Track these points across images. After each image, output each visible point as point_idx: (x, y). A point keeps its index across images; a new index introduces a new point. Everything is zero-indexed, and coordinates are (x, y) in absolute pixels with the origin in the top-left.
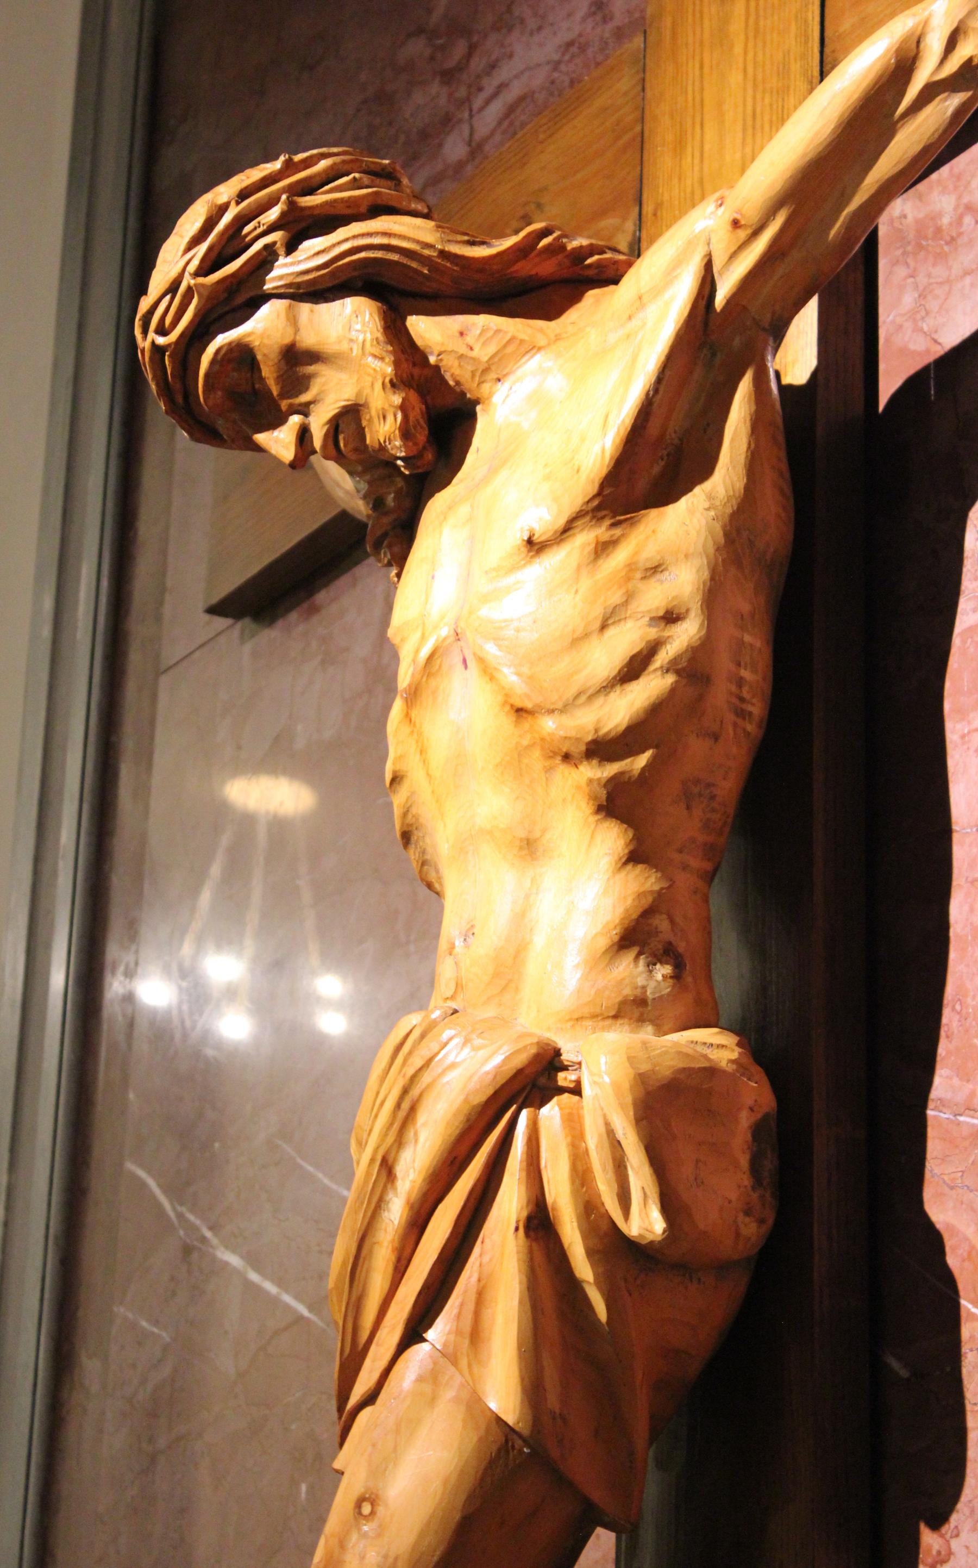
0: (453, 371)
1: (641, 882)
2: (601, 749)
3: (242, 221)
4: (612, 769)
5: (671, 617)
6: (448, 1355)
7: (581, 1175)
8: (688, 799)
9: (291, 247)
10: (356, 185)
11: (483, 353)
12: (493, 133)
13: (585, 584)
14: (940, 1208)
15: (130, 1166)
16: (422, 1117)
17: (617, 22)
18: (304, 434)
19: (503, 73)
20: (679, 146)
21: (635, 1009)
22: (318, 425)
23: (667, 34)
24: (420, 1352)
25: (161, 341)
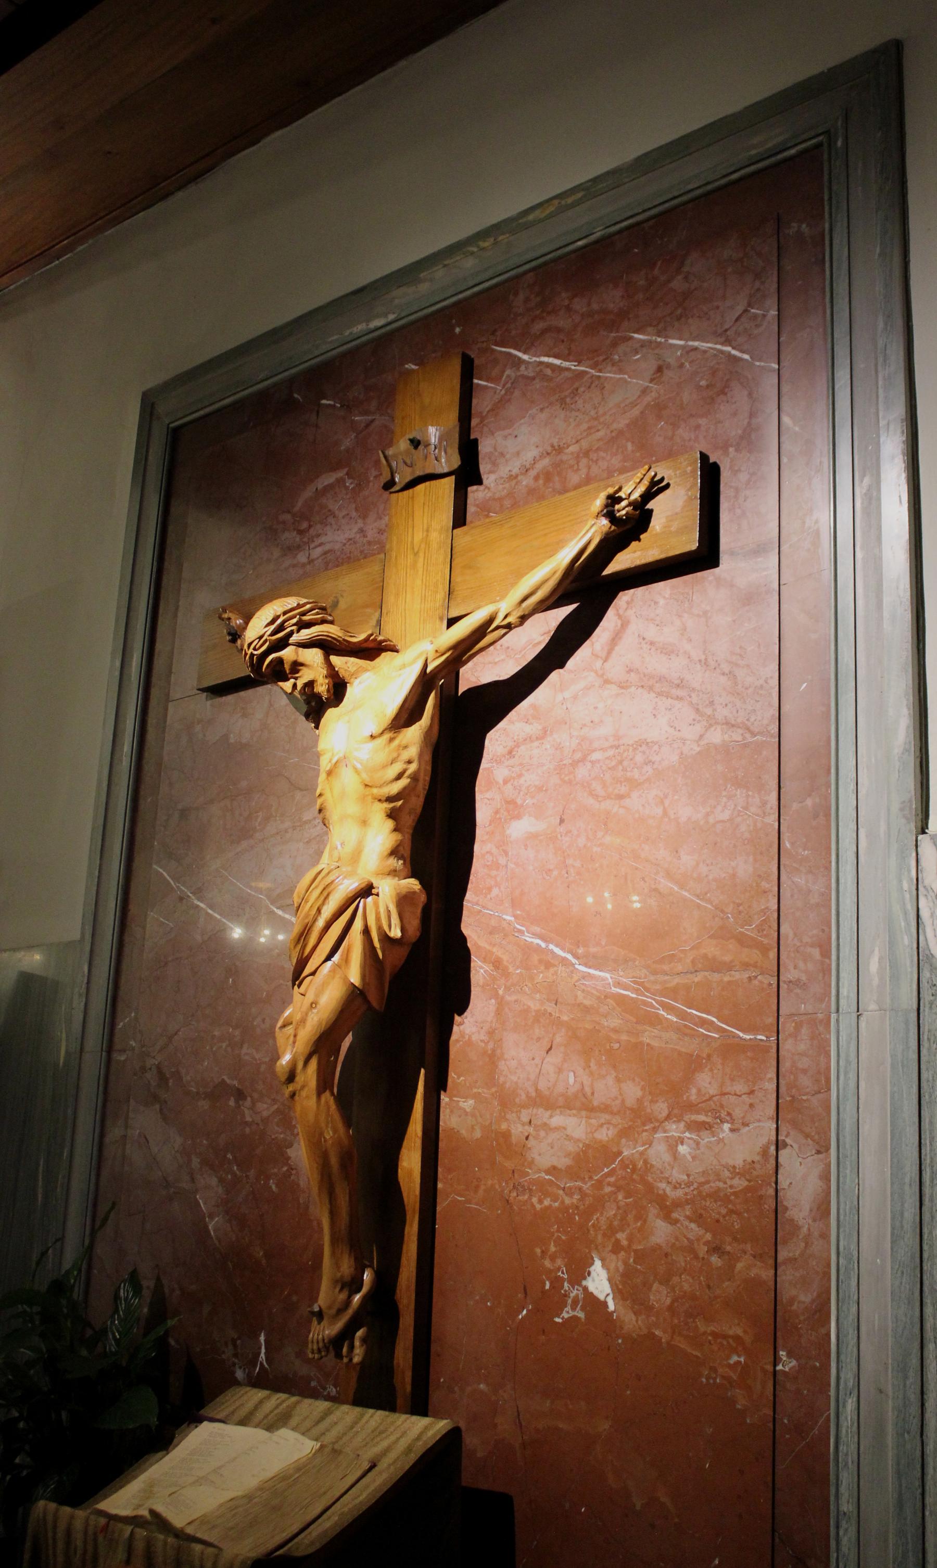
0: (342, 674)
1: (398, 836)
2: (390, 799)
3: (284, 622)
4: (392, 805)
5: (409, 762)
6: (338, 966)
7: (378, 919)
8: (410, 813)
9: (298, 631)
10: (318, 614)
11: (352, 669)
12: (318, 558)
13: (387, 750)
14: (466, 929)
15: (155, 866)
16: (331, 898)
17: (369, 538)
18: (295, 686)
19: (323, 539)
20: (397, 595)
21: (393, 873)
22: (300, 683)
23: (393, 559)
24: (329, 963)
25: (255, 653)
